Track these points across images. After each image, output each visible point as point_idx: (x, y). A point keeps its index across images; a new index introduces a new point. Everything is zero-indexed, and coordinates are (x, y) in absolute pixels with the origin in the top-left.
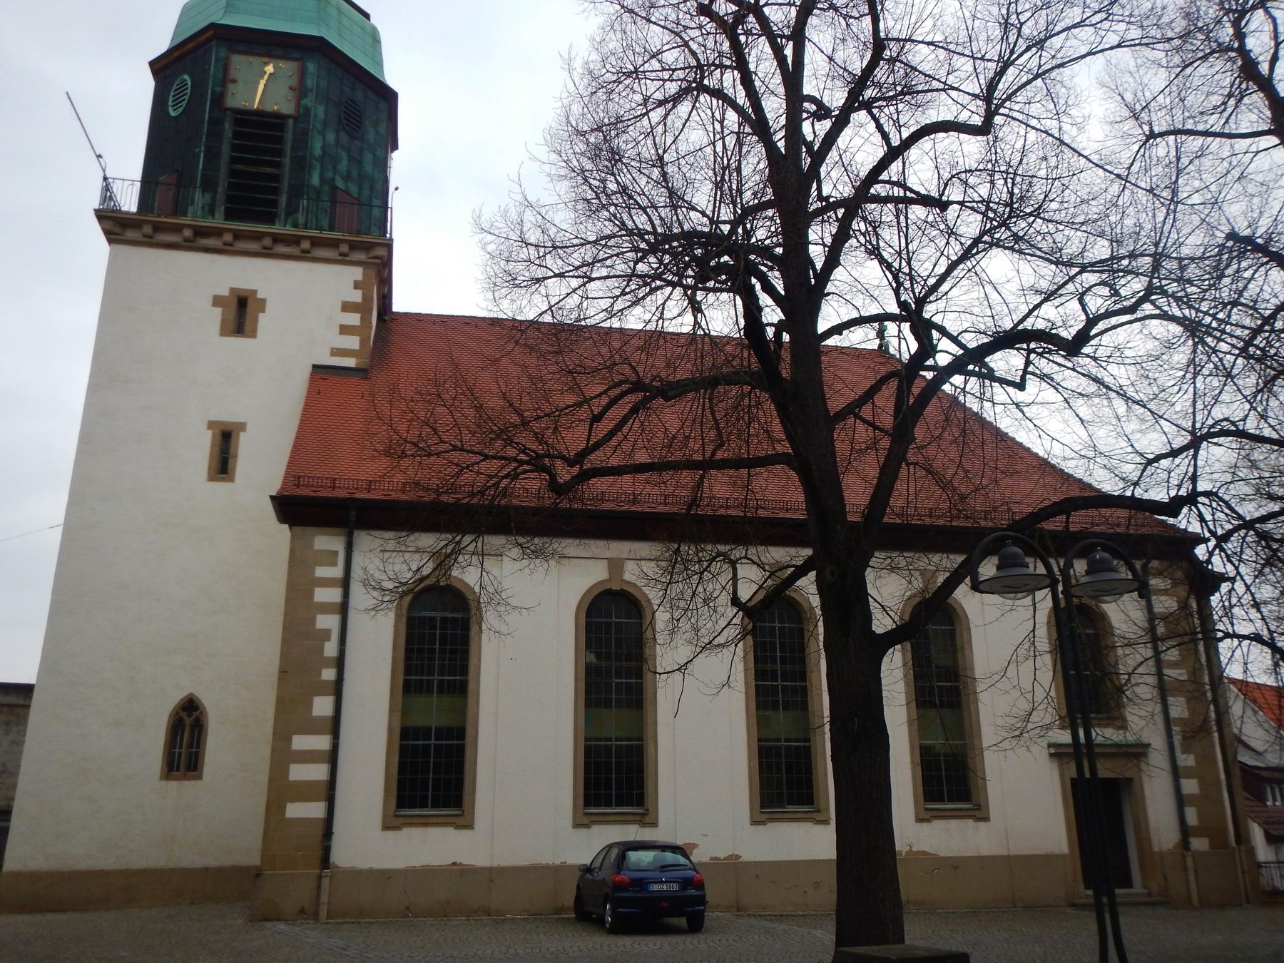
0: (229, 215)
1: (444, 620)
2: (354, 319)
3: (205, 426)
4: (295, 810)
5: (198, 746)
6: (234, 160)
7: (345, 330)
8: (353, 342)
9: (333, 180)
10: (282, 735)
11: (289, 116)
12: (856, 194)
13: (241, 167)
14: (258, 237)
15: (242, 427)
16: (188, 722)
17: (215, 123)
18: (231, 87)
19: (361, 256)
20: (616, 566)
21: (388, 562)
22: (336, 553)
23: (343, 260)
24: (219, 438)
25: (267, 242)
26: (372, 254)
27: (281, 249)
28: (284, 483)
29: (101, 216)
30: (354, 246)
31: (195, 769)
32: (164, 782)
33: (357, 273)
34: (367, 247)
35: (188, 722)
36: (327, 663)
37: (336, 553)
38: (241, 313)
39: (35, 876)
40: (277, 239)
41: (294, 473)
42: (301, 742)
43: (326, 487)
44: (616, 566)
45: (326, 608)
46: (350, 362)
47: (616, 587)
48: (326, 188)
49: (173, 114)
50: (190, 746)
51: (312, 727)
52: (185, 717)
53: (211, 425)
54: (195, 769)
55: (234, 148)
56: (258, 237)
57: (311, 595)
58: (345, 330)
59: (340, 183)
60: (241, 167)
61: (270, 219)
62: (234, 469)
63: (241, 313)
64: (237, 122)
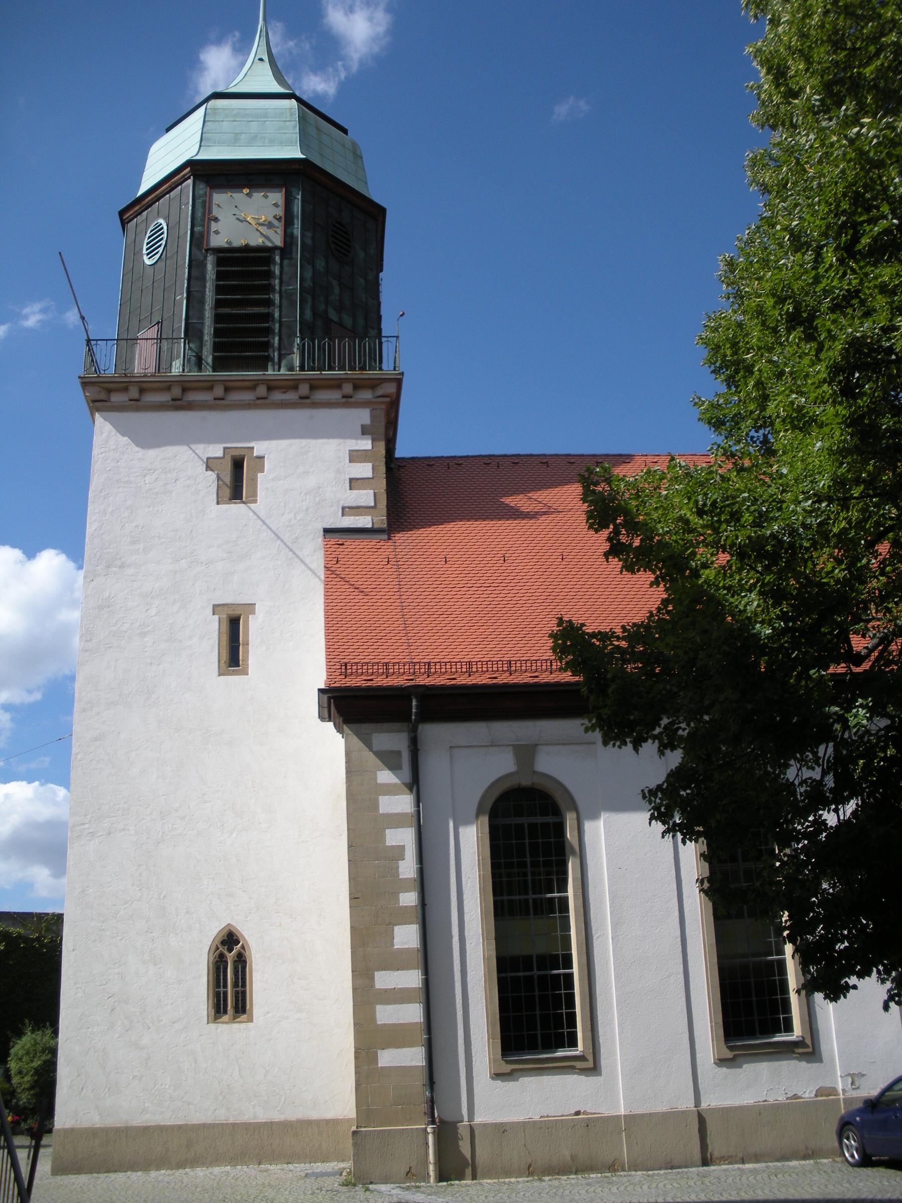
0: (218, 364)
1: (533, 827)
2: (365, 470)
3: (210, 610)
4: (387, 1058)
5: (244, 985)
6: (219, 304)
7: (354, 483)
8: (365, 497)
9: (326, 312)
10: (363, 972)
11: (276, 248)
12: (198, 58)
13: (227, 310)
14: (252, 386)
15: (250, 608)
16: (230, 957)
17: (196, 265)
18: (214, 226)
19: (366, 395)
20: (526, 753)
21: (474, 760)
22: (399, 753)
23: (347, 402)
24: (225, 626)
25: (262, 390)
26: (380, 392)
27: (277, 396)
28: (329, 674)
29: (86, 383)
30: (358, 386)
31: (244, 1011)
32: (213, 1026)
33: (364, 416)
34: (373, 384)
35: (230, 957)
36: (404, 885)
37: (399, 753)
38: (236, 479)
39: (92, 1133)
40: (271, 387)
41: (337, 660)
42: (385, 980)
43: (379, 675)
44: (526, 753)
45: (396, 821)
46: (365, 522)
47: (526, 782)
48: (319, 323)
49: (148, 262)
50: (235, 984)
51: (396, 962)
52: (226, 953)
53: (216, 608)
54: (244, 1011)
55: (219, 290)
56: (252, 386)
57: (376, 806)
58: (354, 483)
59: (333, 315)
60: (227, 310)
61: (262, 363)
62: (246, 659)
63: (236, 479)
64: (220, 262)
